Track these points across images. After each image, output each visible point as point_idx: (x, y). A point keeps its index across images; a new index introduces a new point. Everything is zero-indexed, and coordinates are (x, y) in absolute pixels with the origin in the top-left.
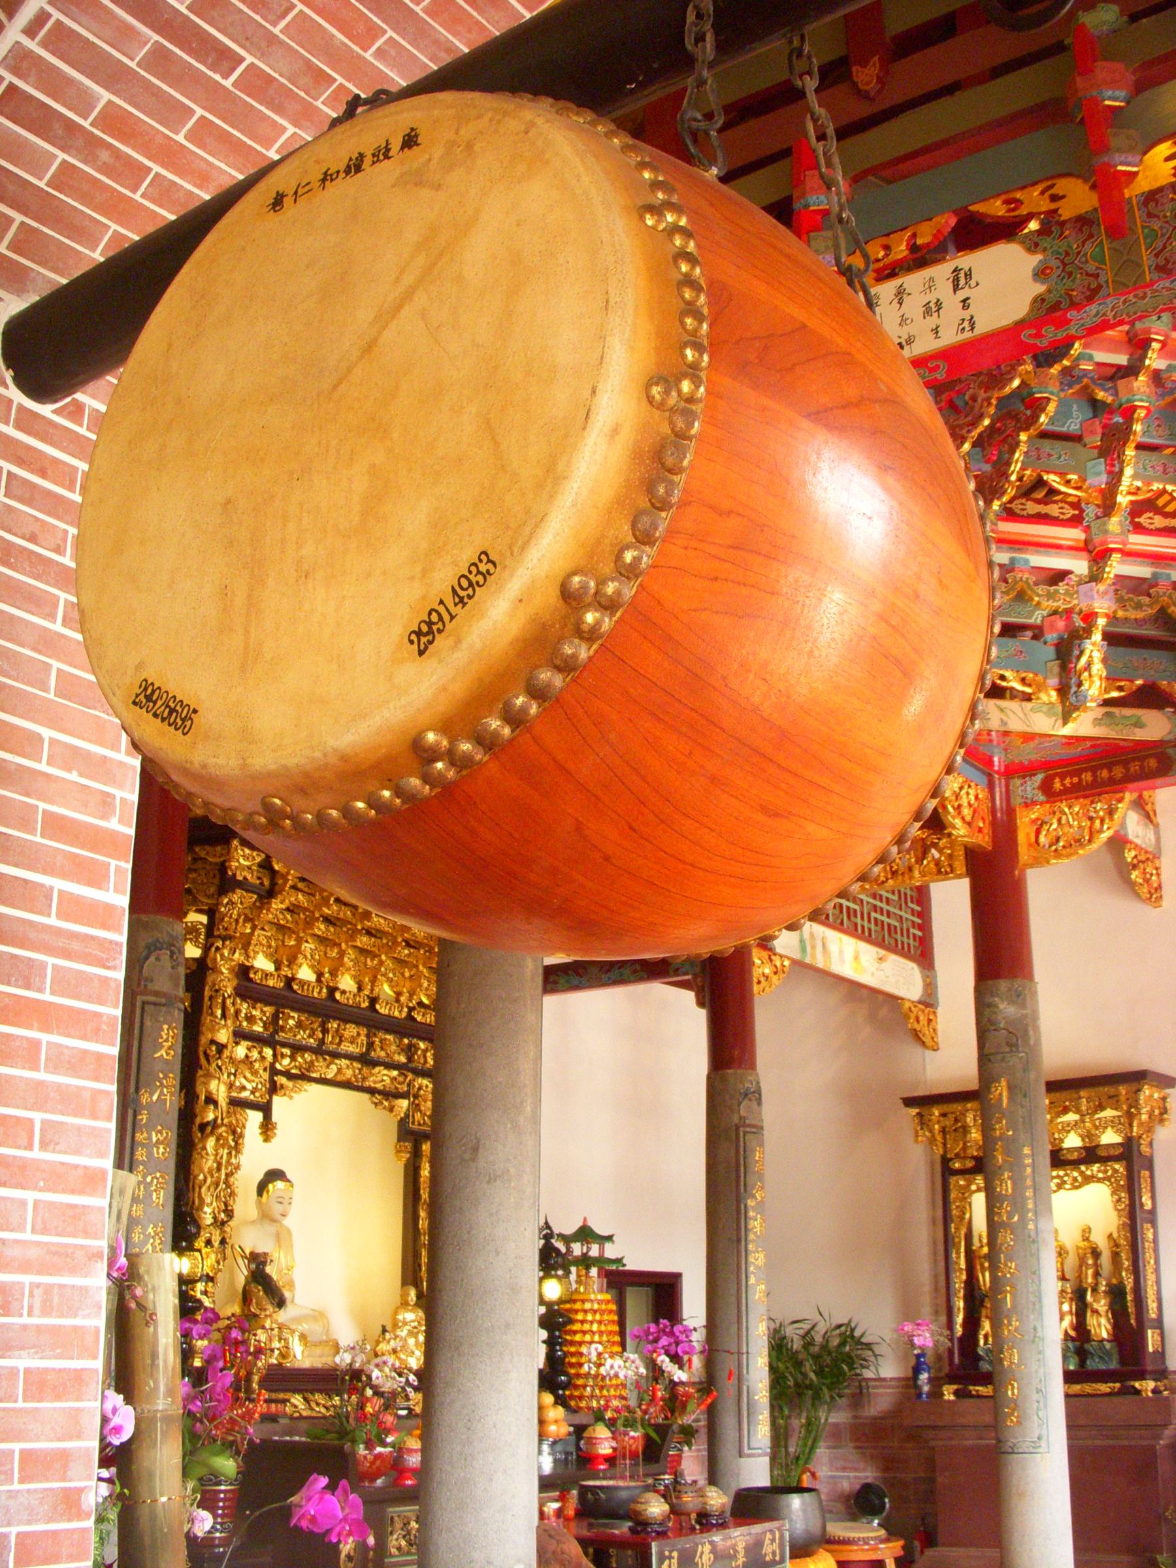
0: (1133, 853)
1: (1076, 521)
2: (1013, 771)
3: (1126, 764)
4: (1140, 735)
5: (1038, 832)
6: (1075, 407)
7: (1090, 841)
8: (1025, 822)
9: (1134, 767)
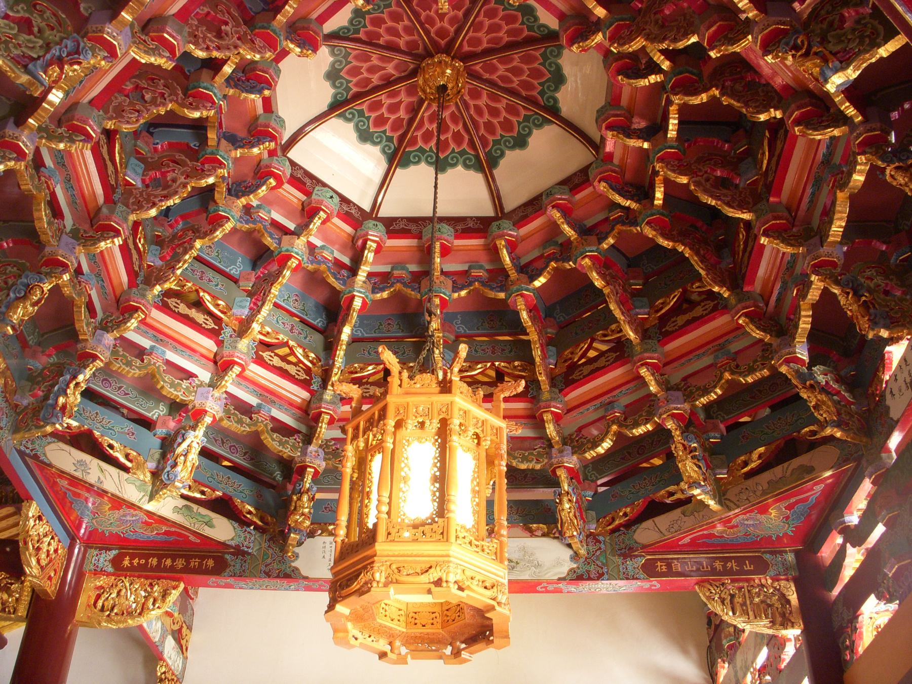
0: (164, 669)
1: (214, 334)
2: (96, 541)
3: (188, 558)
4: (207, 532)
5: (98, 597)
6: (240, 260)
7: (140, 614)
8: (90, 586)
9: (195, 563)
